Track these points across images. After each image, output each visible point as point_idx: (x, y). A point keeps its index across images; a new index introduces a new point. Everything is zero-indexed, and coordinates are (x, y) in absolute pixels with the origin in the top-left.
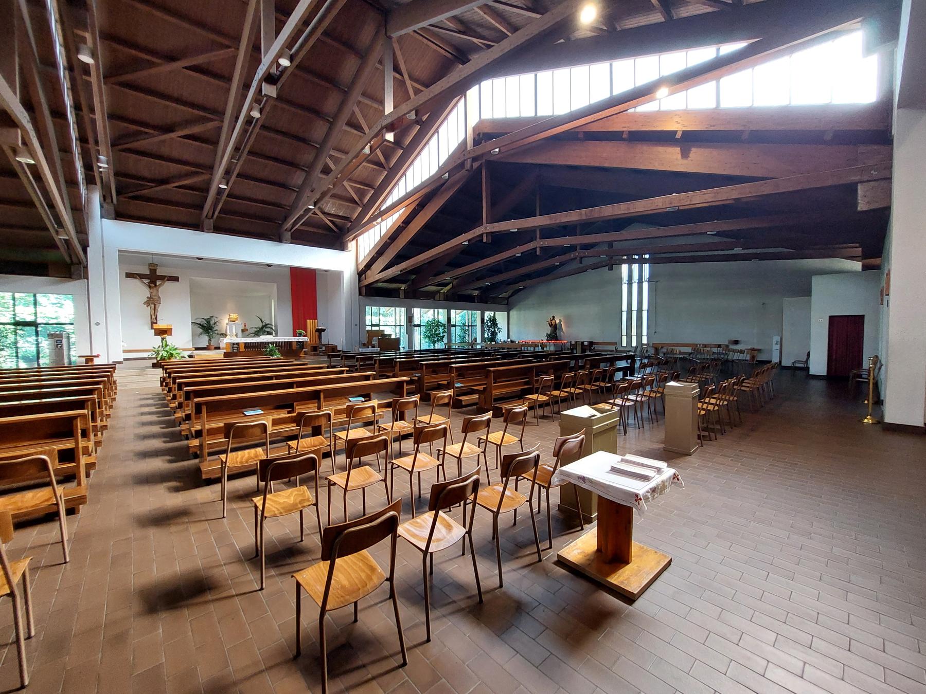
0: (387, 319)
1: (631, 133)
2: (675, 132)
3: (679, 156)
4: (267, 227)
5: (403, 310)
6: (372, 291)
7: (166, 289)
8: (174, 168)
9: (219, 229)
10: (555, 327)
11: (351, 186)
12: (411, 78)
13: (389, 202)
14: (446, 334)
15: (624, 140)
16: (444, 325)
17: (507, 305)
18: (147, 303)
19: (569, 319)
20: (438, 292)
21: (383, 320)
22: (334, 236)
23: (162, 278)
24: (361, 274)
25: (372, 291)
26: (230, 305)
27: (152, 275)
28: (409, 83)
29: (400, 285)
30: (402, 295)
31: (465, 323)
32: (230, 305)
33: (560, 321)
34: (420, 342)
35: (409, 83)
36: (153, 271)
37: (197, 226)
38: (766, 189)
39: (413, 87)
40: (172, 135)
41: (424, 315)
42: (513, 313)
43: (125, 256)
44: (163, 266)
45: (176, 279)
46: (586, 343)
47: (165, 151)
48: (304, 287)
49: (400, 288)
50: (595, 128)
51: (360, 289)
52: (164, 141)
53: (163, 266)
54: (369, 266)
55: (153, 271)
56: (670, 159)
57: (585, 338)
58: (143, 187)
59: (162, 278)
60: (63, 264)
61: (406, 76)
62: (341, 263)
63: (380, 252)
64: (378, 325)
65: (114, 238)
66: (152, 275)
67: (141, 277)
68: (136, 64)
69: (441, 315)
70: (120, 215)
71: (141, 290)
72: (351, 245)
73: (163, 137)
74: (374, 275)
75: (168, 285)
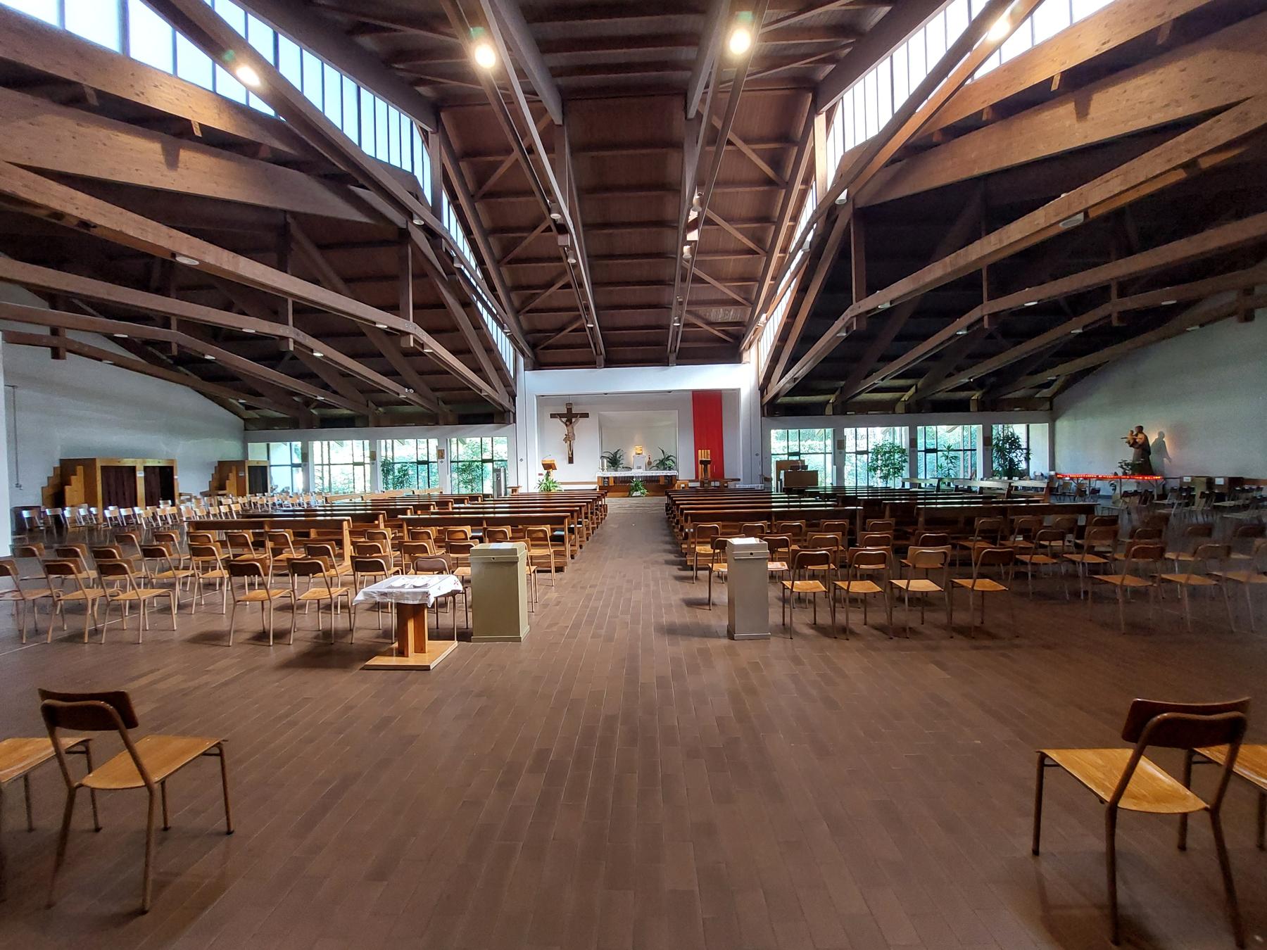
0: (810, 446)
1: (995, 107)
2: (1051, 80)
3: (1074, 121)
4: (654, 353)
5: (905, 429)
6: (777, 409)
7: (580, 424)
8: (565, 316)
9: (610, 362)
10: (1143, 449)
11: (729, 288)
12: (747, 141)
13: (789, 293)
14: (906, 465)
15: (986, 124)
16: (903, 451)
17: (1047, 408)
18: (565, 440)
19: (1181, 434)
20: (899, 400)
21: (805, 446)
22: (727, 348)
23: (576, 415)
24: (763, 388)
25: (777, 409)
26: (637, 438)
27: (570, 414)
28: (745, 149)
29: (828, 397)
30: (973, 407)
31: (951, 451)
32: (637, 438)
33: (1161, 435)
34: (858, 477)
35: (745, 149)
36: (569, 410)
37: (590, 363)
38: (1222, 131)
39: (754, 150)
40: (553, 289)
41: (869, 437)
42: (1063, 425)
43: (543, 400)
44: (577, 404)
45: (586, 415)
46: (1220, 481)
47: (555, 304)
48: (708, 411)
49: (828, 402)
50: (952, 118)
51: (762, 407)
52: (550, 296)
53: (577, 404)
54: (768, 377)
55: (569, 410)
56: (1060, 130)
57: (1221, 469)
58: (550, 338)
59: (576, 415)
60: (491, 413)
61: (739, 143)
62: (739, 378)
63: (775, 359)
64: (798, 454)
65: (536, 385)
66: (570, 414)
67: (561, 416)
68: (516, 243)
69: (900, 436)
70: (538, 364)
71: (559, 427)
72: (745, 356)
73: (548, 293)
74: (775, 387)
75: (581, 420)
